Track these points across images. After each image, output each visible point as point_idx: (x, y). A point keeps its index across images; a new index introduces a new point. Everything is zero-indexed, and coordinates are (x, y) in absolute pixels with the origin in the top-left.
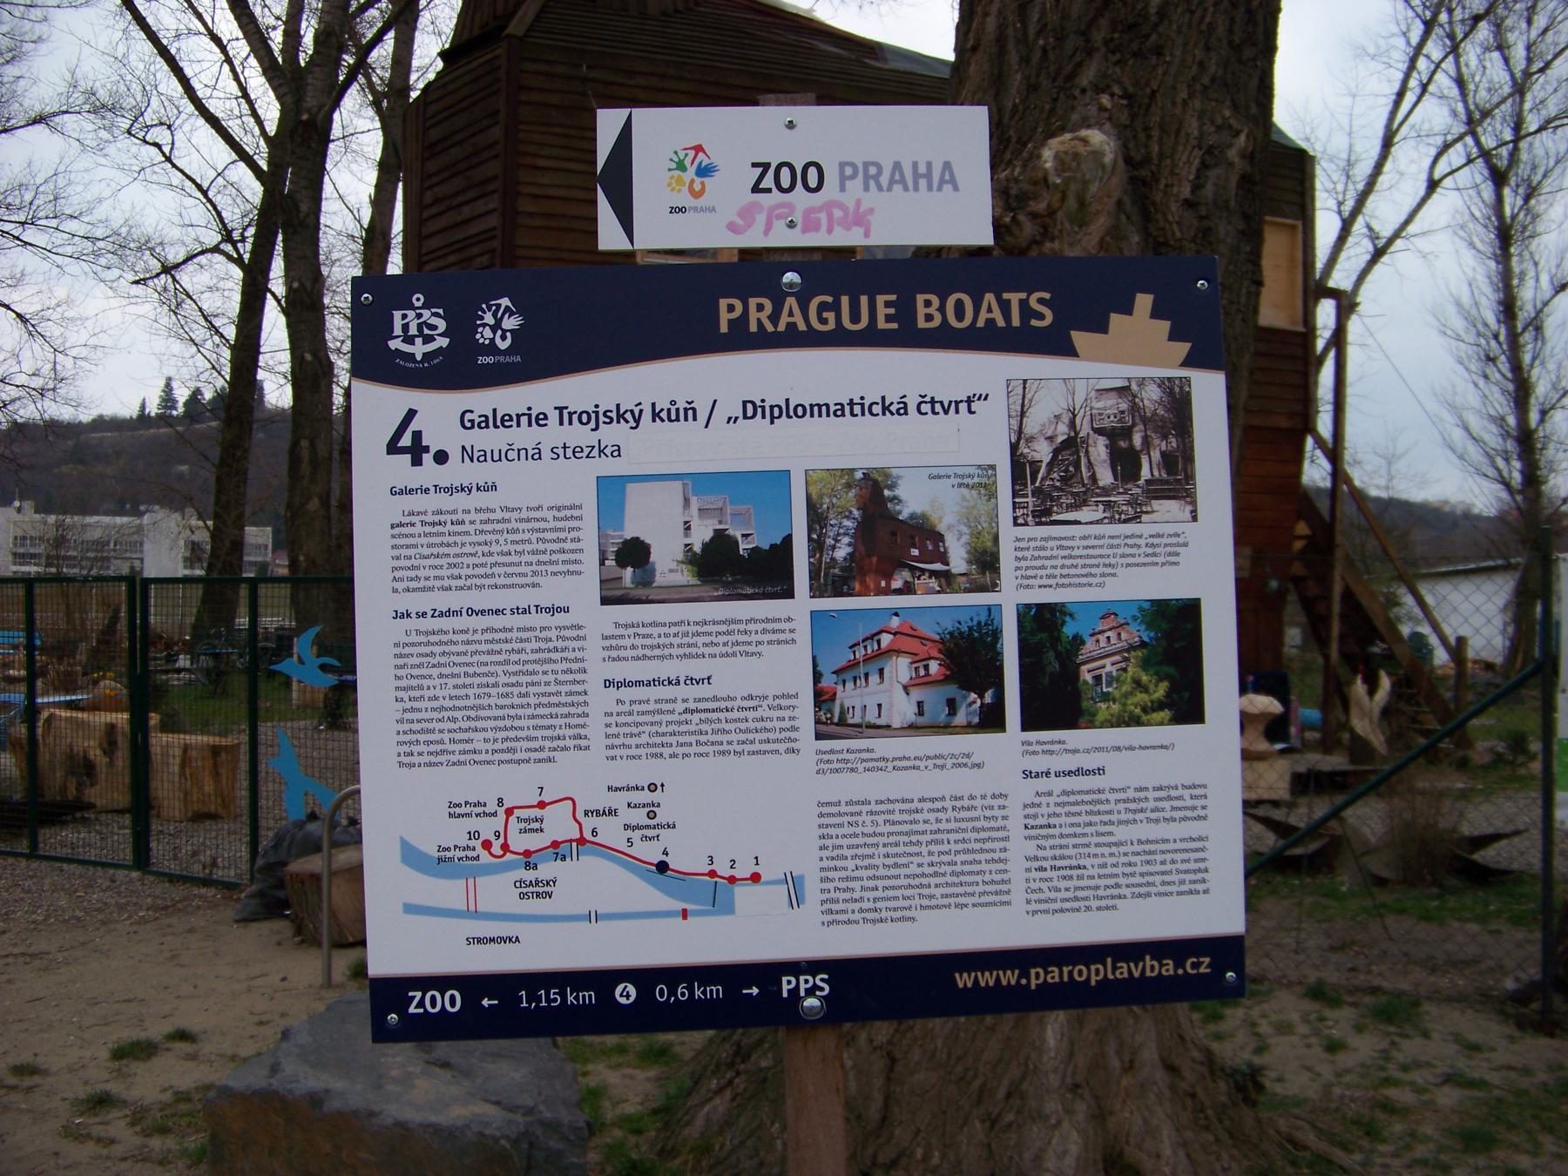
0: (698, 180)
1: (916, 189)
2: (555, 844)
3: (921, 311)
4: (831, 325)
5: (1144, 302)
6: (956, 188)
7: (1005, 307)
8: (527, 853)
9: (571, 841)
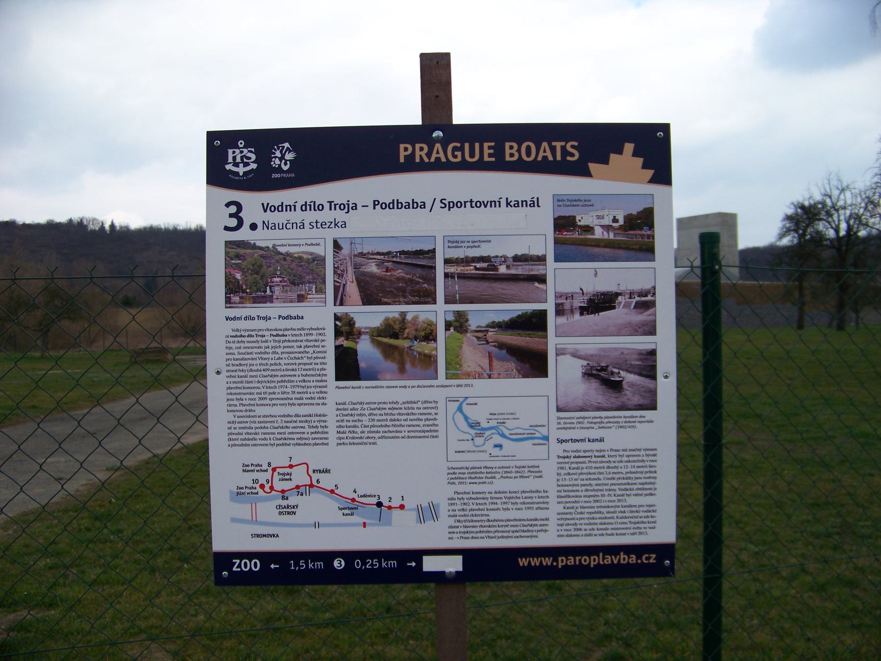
2: (298, 487)
3: (508, 151)
5: (629, 147)
7: (553, 150)
8: (283, 491)
9: (306, 485)
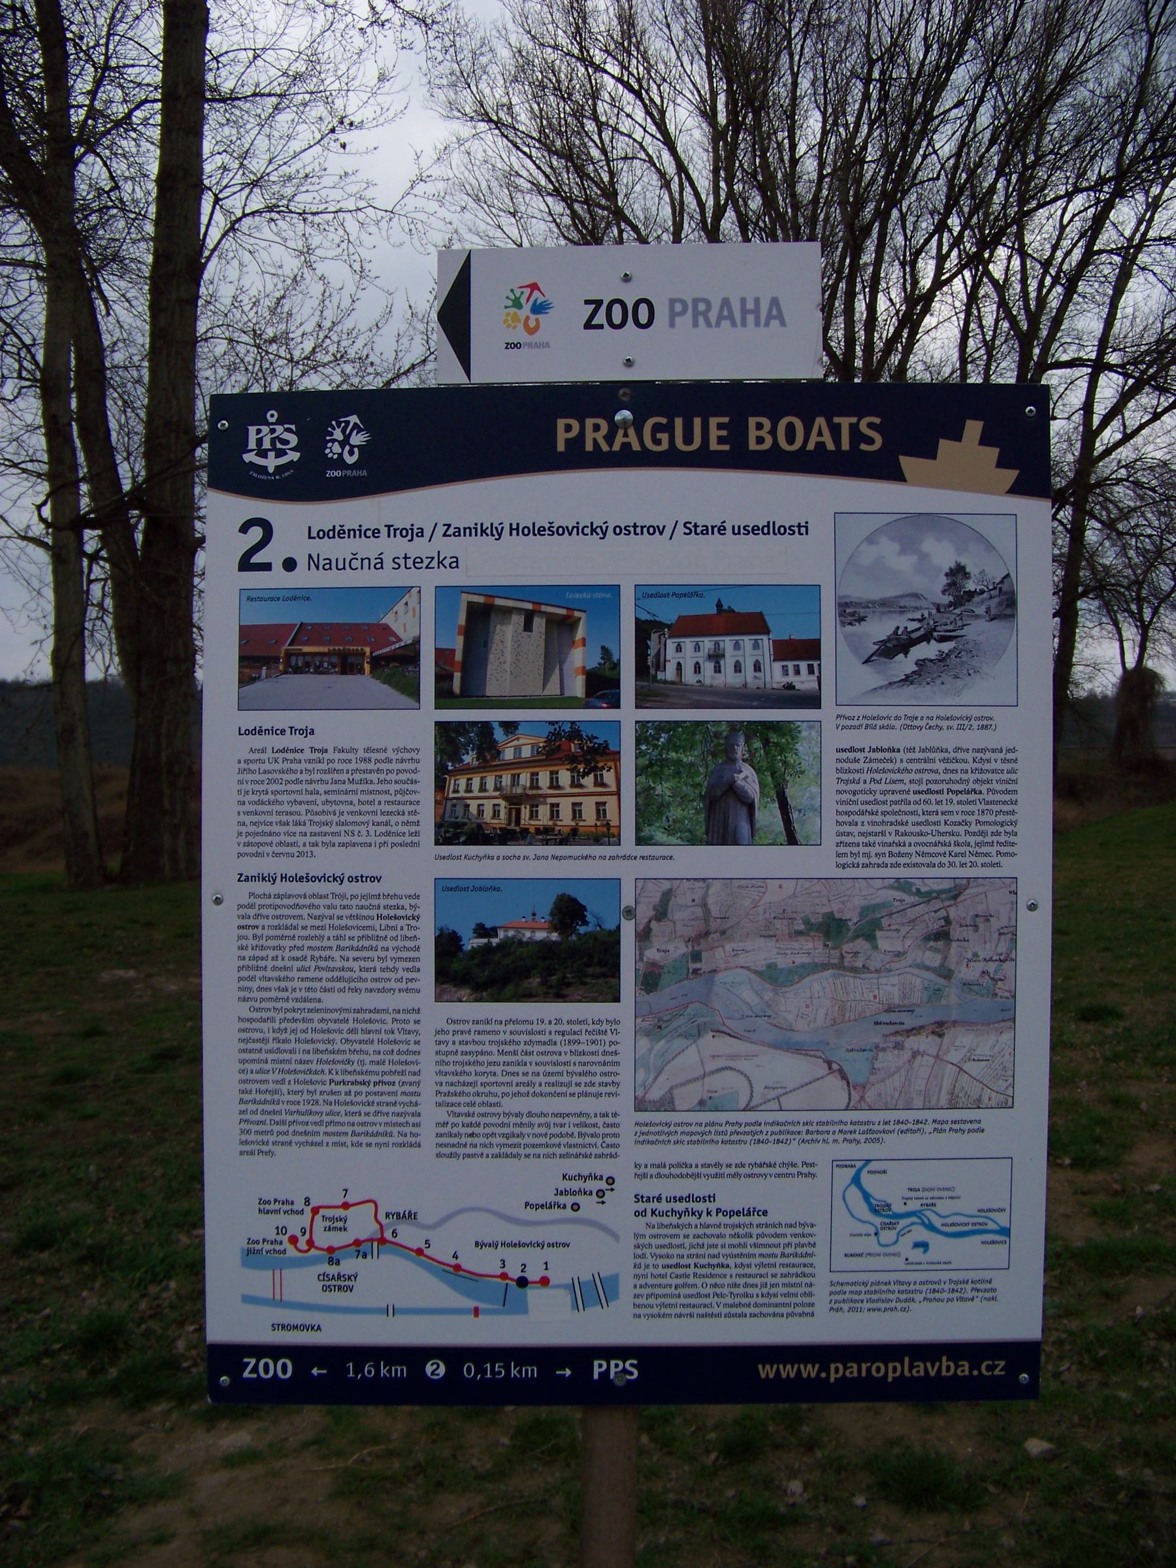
0: (533, 317)
1: (744, 324)
2: (357, 1242)
3: (753, 433)
4: (665, 446)
6: (783, 324)
7: (835, 431)
8: (331, 1250)
9: (371, 1240)
